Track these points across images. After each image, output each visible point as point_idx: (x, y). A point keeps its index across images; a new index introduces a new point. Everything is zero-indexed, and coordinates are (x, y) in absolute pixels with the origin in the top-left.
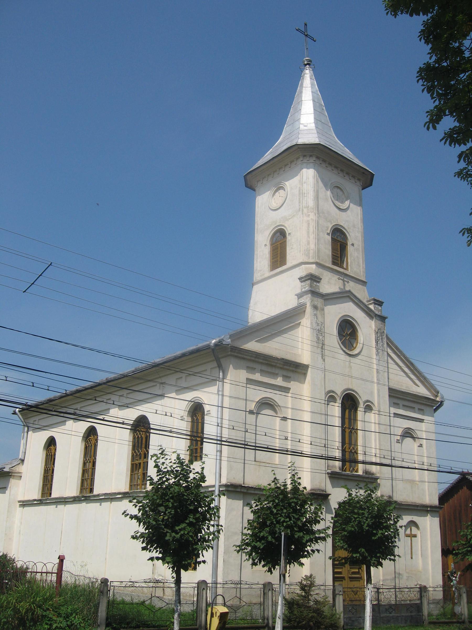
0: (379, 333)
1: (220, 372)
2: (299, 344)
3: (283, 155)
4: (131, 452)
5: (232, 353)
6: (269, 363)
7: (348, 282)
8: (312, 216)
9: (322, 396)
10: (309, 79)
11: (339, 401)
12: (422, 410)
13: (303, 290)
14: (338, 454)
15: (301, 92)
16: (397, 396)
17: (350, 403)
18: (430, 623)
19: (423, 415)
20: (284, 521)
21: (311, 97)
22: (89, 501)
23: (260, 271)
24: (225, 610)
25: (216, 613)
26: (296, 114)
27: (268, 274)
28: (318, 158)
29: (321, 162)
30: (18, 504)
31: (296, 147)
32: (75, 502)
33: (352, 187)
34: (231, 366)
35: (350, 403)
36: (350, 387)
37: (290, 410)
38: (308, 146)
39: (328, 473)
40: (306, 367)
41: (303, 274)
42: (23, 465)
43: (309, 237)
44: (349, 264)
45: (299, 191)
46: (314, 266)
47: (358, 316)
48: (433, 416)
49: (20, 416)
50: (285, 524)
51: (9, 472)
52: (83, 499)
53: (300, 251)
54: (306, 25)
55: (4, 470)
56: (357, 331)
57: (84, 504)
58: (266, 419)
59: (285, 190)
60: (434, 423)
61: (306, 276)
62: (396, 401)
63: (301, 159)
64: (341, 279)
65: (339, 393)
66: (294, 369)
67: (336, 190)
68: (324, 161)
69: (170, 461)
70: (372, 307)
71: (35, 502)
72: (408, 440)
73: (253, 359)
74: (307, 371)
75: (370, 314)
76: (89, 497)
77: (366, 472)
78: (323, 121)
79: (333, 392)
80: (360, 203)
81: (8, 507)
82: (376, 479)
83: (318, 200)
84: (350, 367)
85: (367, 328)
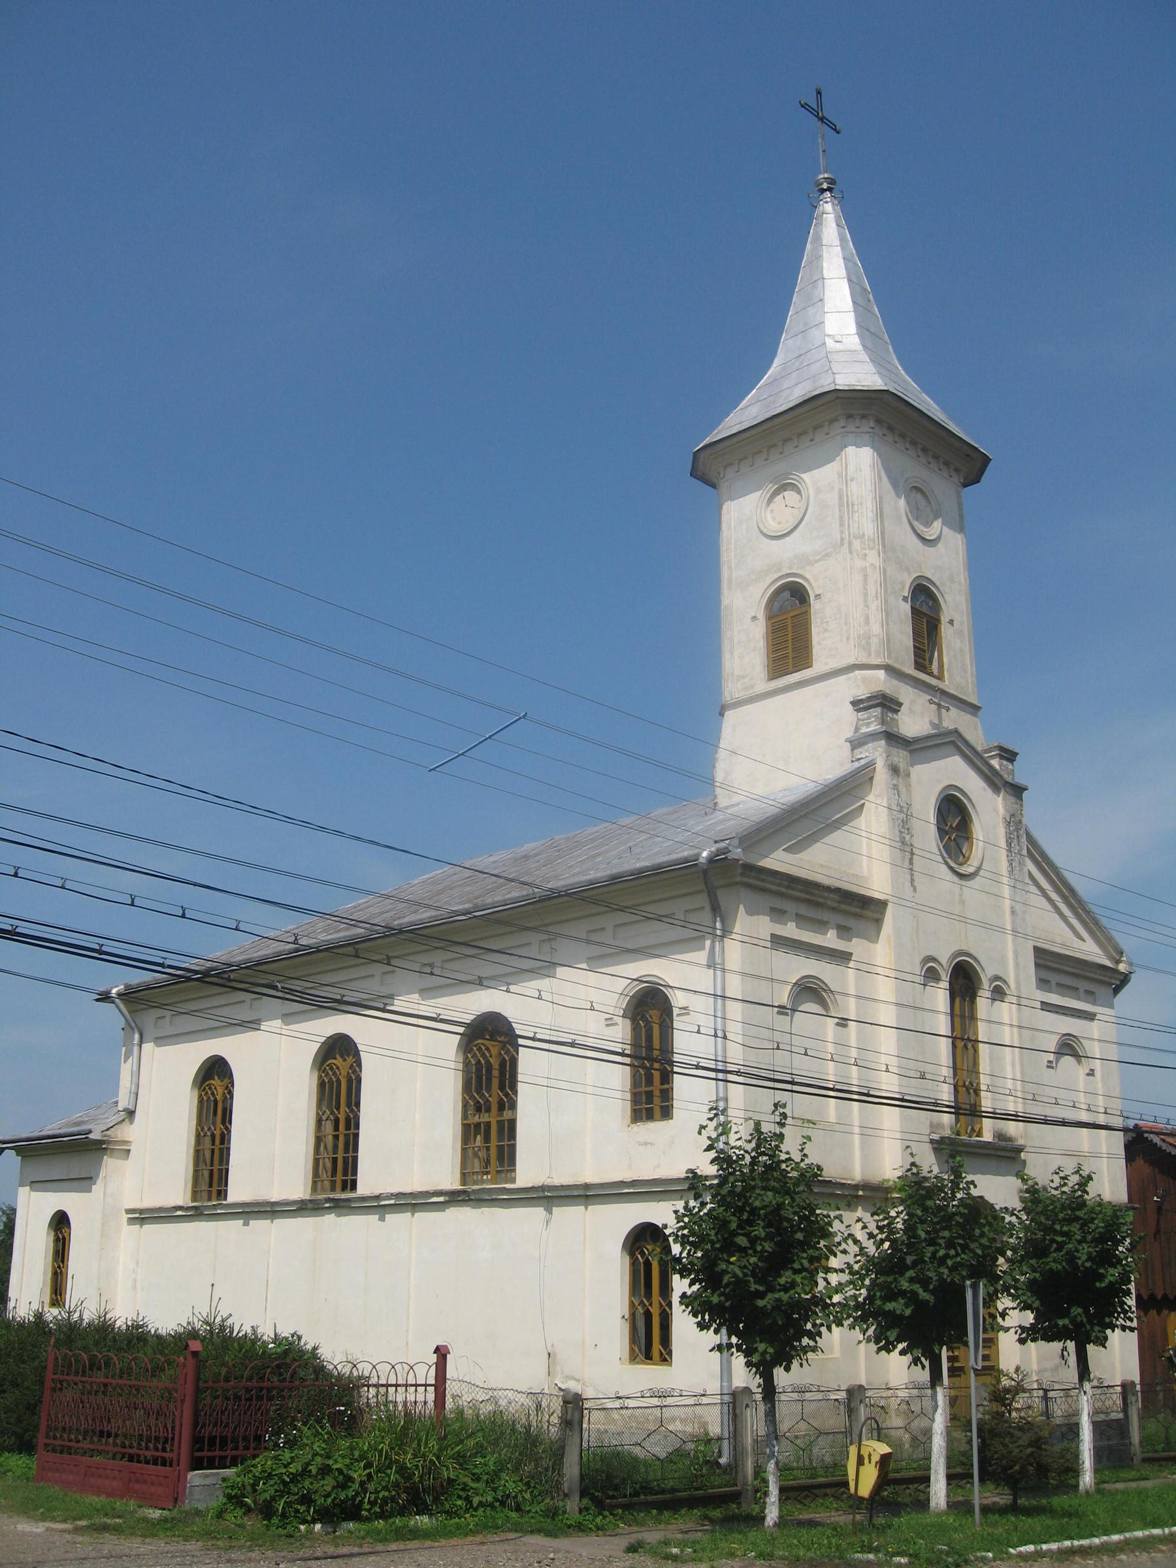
0: (1014, 823)
1: (715, 922)
2: (863, 852)
3: (801, 410)
4: (460, 1097)
5: (745, 880)
6: (814, 898)
7: (948, 710)
8: (873, 558)
9: (916, 968)
10: (834, 225)
11: (945, 977)
12: (1092, 993)
13: (864, 730)
14: (945, 1094)
15: (819, 258)
16: (1052, 966)
17: (964, 981)
18: (1145, 1460)
19: (1094, 1004)
20: (947, 1256)
21: (843, 273)
22: (345, 1211)
23: (743, 677)
24: (885, 1449)
25: (870, 1455)
26: (811, 310)
27: (762, 686)
28: (879, 421)
29: (885, 431)
30: (125, 1217)
31: (833, 396)
32: (305, 1212)
33: (942, 486)
34: (741, 907)
35: (964, 981)
36: (964, 948)
37: (852, 1002)
38: (859, 395)
39: (932, 1141)
40: (882, 905)
41: (863, 693)
42: (131, 1122)
43: (867, 606)
44: (946, 667)
45: (840, 497)
46: (881, 674)
47: (973, 785)
48: (1111, 1007)
49: (122, 1006)
50: (950, 1262)
51: (101, 1142)
52: (327, 1205)
53: (848, 638)
54: (819, 93)
55: (91, 1136)
56: (971, 820)
57: (330, 1219)
58: (807, 1021)
59: (799, 492)
60: (1113, 1020)
61: (869, 699)
62: (1046, 975)
63: (842, 423)
64: (934, 703)
65: (944, 960)
66: (858, 910)
67: (914, 494)
68: (891, 429)
69: (738, 1136)
70: (995, 763)
71: (179, 1213)
72: (1068, 1060)
73: (784, 890)
74: (883, 913)
75: (994, 781)
76: (348, 1200)
77: (1000, 1136)
78: (872, 330)
79: (934, 959)
80: (960, 526)
81: (103, 1224)
82: (1020, 1150)
83: (882, 521)
84: (962, 902)
85: (989, 812)
